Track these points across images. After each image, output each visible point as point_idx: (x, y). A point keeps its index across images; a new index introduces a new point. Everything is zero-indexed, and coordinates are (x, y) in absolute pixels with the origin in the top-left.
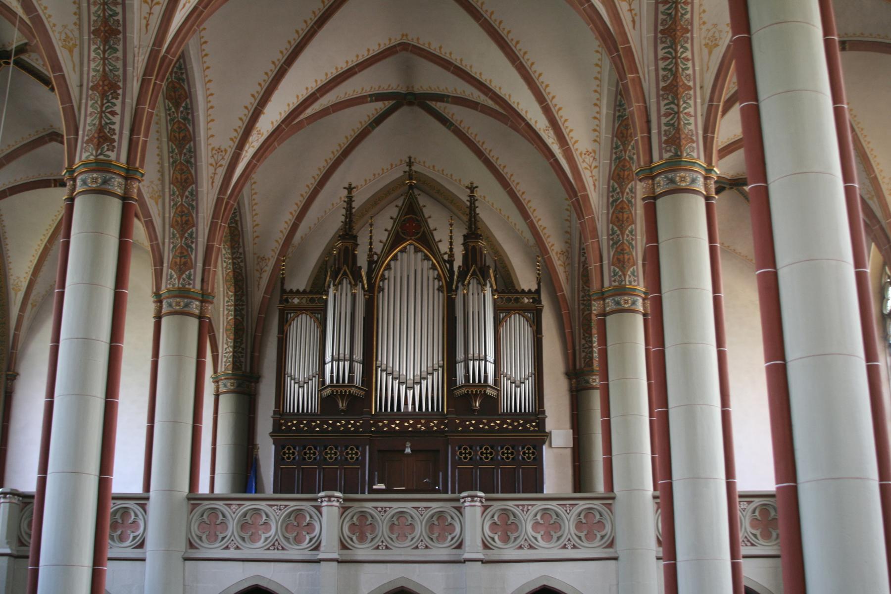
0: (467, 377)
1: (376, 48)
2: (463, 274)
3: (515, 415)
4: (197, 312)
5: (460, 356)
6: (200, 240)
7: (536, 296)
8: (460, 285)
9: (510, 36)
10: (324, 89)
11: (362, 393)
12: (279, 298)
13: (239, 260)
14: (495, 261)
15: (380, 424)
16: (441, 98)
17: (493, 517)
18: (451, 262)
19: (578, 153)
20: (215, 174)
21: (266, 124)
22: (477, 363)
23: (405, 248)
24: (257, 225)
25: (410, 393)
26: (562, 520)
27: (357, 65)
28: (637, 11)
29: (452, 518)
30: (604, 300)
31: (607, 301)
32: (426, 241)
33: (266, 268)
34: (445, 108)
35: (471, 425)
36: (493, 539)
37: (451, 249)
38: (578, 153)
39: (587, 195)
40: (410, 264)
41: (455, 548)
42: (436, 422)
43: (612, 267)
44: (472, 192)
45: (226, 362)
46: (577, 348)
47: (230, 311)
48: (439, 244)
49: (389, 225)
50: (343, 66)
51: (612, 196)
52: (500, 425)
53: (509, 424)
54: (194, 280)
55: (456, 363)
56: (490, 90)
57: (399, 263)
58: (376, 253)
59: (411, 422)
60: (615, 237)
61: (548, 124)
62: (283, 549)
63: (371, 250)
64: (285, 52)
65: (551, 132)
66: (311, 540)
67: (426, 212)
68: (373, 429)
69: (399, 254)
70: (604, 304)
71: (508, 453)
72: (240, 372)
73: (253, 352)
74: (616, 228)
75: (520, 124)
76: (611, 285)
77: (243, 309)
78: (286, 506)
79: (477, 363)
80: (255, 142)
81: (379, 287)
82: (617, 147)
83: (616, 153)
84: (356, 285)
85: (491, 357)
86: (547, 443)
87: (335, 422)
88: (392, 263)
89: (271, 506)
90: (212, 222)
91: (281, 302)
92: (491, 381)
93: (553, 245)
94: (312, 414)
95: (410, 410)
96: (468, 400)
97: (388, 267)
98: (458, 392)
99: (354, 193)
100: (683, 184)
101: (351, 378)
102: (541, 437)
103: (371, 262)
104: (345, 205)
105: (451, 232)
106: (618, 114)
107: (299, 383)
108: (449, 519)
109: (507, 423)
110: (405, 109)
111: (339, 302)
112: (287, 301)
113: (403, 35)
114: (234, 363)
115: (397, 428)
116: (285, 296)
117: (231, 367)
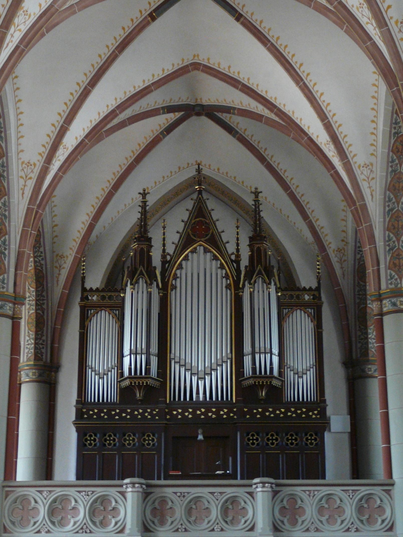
0: (254, 369)
1: (170, 68)
2: (250, 273)
3: (298, 404)
4: (10, 313)
5: (247, 348)
6: (13, 246)
7: (316, 293)
8: (246, 283)
9: (295, 59)
10: (122, 107)
11: (157, 384)
12: (80, 296)
13: (40, 259)
14: (278, 262)
15: (175, 413)
16: (228, 110)
17: (282, 501)
18: (238, 261)
19: (357, 165)
20: (25, 186)
21: (71, 140)
22: (262, 356)
23: (195, 248)
24: (56, 225)
25: (201, 383)
26: (346, 504)
27: (153, 84)
28: (374, 188)
29: (245, 502)
30: (381, 301)
31: (384, 302)
32: (214, 242)
33: (65, 265)
34: (230, 118)
35: (258, 413)
36: (282, 522)
37: (238, 250)
38: (357, 165)
39: (365, 204)
40: (199, 264)
41: (248, 531)
42: (226, 410)
43: (389, 271)
44: (257, 196)
45: (28, 353)
46: (354, 339)
47: (31, 305)
48: (227, 245)
49: (181, 227)
50: (140, 85)
51: (389, 206)
52: (285, 413)
53: (293, 413)
54: (7, 284)
55: (243, 356)
56: (275, 106)
57: (189, 263)
58: (168, 254)
59: (203, 410)
60: (391, 243)
61: (329, 140)
62: (91, 532)
63: (164, 251)
64: (88, 74)
65: (332, 147)
66: (116, 523)
67: (215, 215)
68: (168, 417)
69: (190, 254)
70: (381, 305)
71: (292, 439)
72: (41, 363)
73: (53, 343)
74: (392, 235)
75: (303, 139)
76: (387, 288)
77: (43, 304)
78: (93, 492)
79: (262, 356)
80: (62, 155)
81: (172, 285)
82: (393, 161)
83: (392, 167)
84: (151, 284)
85: (275, 350)
86: (327, 429)
87: (133, 411)
88: (184, 263)
89: (79, 492)
90: (23, 230)
91: (82, 299)
92: (276, 373)
93: (330, 243)
94: (111, 403)
95: (201, 399)
96: (257, 392)
97: (180, 267)
98: (246, 383)
99: (148, 197)
100: (370, 373)
101: (148, 370)
102: (324, 424)
103: (164, 262)
104: (140, 209)
105: (238, 234)
106: (393, 131)
107: (99, 374)
108: (243, 503)
109: (290, 411)
110: (194, 119)
111: (134, 299)
112: (87, 298)
113: (194, 56)
114: (36, 354)
115: (190, 416)
116: (85, 294)
117: (33, 358)
